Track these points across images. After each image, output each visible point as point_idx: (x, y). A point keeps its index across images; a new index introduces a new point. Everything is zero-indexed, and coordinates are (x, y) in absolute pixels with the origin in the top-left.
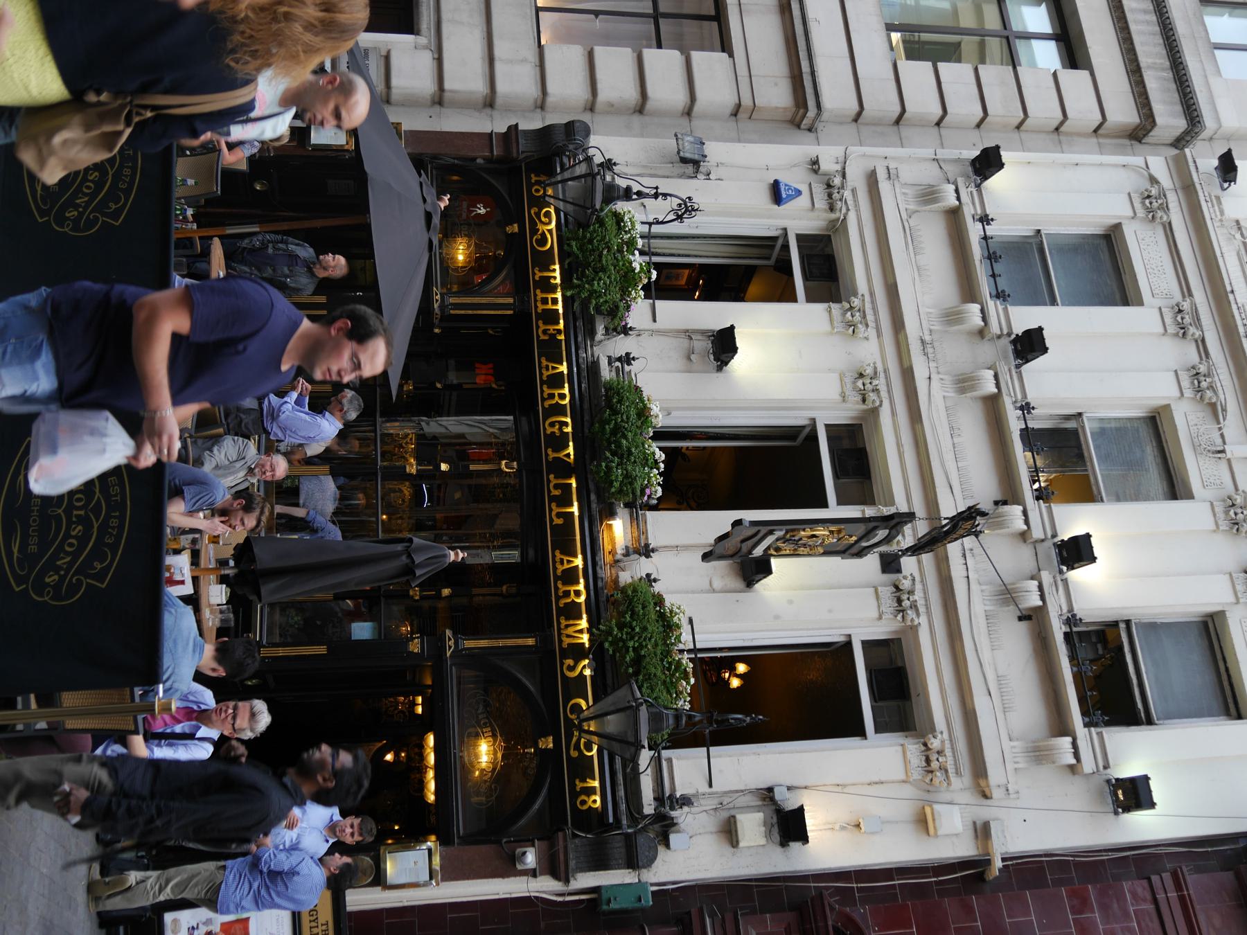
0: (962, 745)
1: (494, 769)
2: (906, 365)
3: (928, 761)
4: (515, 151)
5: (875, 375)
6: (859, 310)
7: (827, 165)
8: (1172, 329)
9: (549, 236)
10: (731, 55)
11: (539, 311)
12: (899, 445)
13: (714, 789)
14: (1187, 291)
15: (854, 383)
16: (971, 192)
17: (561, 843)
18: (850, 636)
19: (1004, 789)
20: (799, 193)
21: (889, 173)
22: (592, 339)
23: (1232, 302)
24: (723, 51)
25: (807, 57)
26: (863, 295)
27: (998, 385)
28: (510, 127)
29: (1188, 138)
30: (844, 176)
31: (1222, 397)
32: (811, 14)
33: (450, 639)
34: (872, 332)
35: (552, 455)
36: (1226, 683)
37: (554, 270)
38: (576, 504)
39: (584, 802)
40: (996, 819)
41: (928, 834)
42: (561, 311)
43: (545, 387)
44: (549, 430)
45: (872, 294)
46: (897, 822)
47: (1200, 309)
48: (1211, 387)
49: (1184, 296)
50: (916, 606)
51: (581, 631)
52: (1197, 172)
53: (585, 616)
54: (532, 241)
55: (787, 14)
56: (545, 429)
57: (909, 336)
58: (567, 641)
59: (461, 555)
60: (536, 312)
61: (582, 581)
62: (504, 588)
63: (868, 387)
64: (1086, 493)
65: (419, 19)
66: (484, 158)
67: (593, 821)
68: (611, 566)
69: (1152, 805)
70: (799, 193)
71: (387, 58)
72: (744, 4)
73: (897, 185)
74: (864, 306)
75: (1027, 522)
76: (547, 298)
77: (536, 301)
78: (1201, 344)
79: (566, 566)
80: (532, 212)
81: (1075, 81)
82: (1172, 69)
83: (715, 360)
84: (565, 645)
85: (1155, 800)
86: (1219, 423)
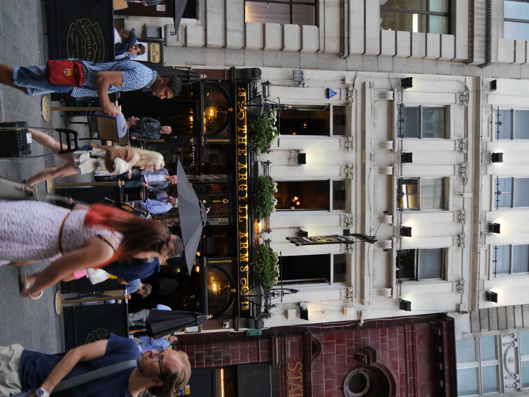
0: (358, 289)
1: (214, 117)
2: (363, 162)
3: (347, 295)
4: (233, 79)
5: (352, 168)
6: (351, 142)
7: (348, 81)
8: (457, 149)
9: (243, 114)
10: (318, 27)
11: (239, 199)
12: (356, 192)
13: (282, 303)
14: (466, 135)
15: (345, 170)
16: (399, 94)
17: (236, 321)
18: (329, 104)
19: (368, 303)
20: (336, 93)
21: (370, 85)
22: (256, 153)
23: (481, 140)
24: (316, 25)
25: (347, 30)
26: (353, 136)
27: (393, 172)
28: (231, 68)
29: (484, 66)
30: (353, 85)
31: (467, 176)
32: (352, 9)
33: (205, 261)
34: (354, 150)
35: (240, 198)
36: (443, 268)
37: (245, 128)
38: (247, 215)
39: (243, 308)
40: (363, 310)
41: (344, 314)
42: (246, 144)
43: (239, 173)
44: (240, 189)
45: (356, 216)
46: (335, 311)
47: (469, 144)
48: (465, 172)
49: (465, 137)
50: (352, 248)
51: (246, 257)
52: (483, 86)
53: (247, 253)
54: (237, 116)
55: (342, 8)
56: (238, 189)
57: (366, 152)
58: (241, 260)
59: (205, 76)
60: (239, 262)
61: (247, 241)
62: (223, 236)
63: (349, 172)
64: (416, 134)
65: (198, 11)
66: (221, 80)
67: (246, 314)
68: (257, 234)
69: (410, 236)
70: (336, 93)
71: (186, 29)
72: (327, 37)
73: (372, 90)
74: (352, 140)
75: (393, 221)
76: (242, 139)
77: (238, 140)
78: (466, 156)
79: (243, 236)
80: (238, 104)
81: (448, 39)
82: (486, 4)
83: (298, 162)
84: (241, 262)
85: (412, 235)
86: (464, 185)
